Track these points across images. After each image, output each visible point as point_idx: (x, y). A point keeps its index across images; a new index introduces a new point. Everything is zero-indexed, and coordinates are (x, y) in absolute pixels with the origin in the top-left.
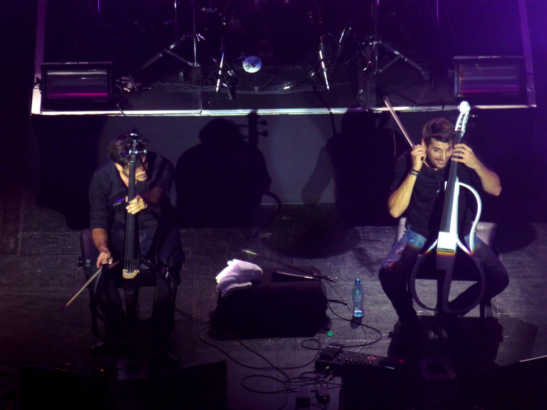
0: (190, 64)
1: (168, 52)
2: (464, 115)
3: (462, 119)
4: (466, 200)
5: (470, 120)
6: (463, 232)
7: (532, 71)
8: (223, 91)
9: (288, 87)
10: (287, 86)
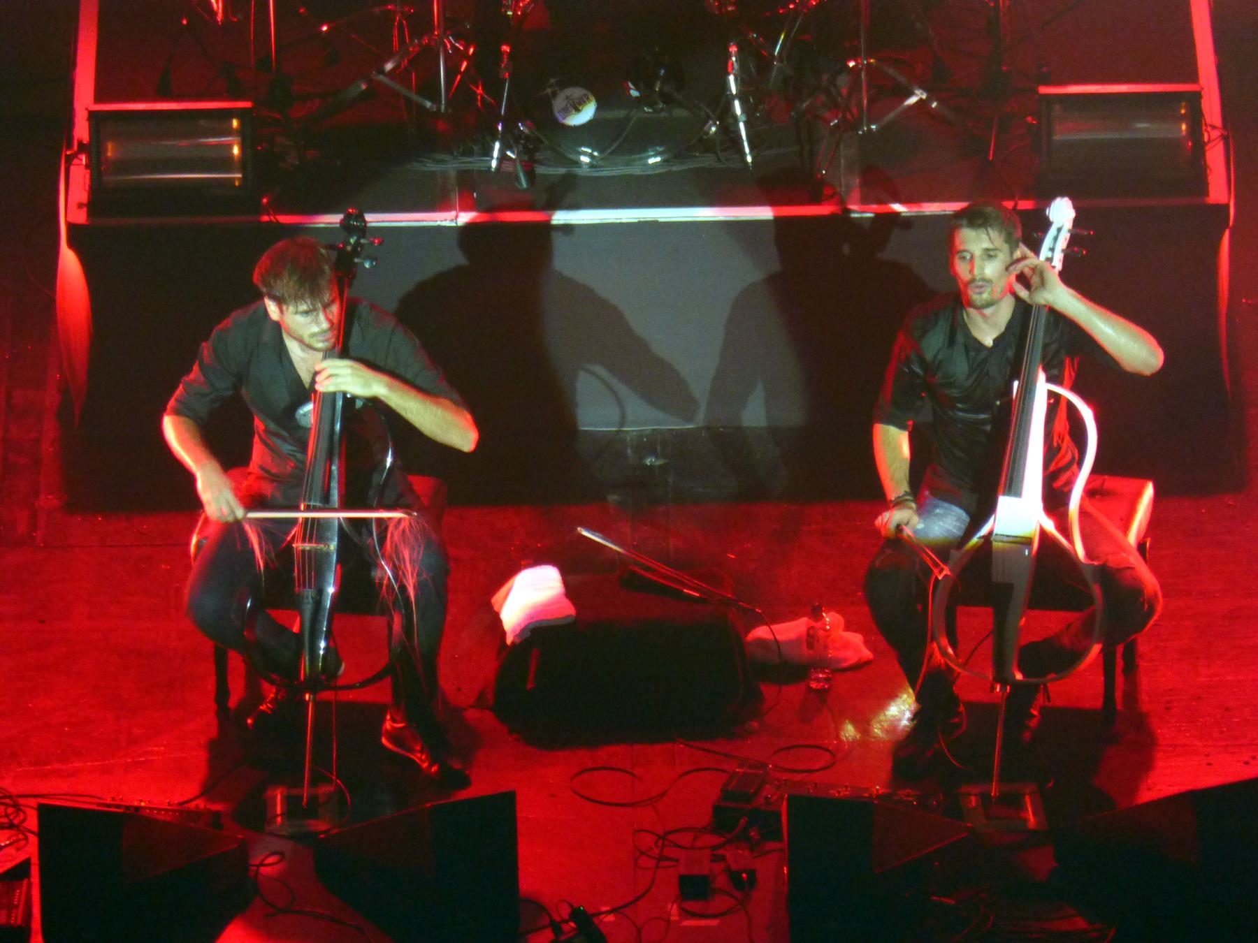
0: (428, 104)
1: (381, 77)
2: (1059, 230)
3: (1056, 239)
5: (1074, 241)
6: (1054, 500)
7: (1217, 121)
8: (508, 167)
9: (658, 159)
10: (655, 156)
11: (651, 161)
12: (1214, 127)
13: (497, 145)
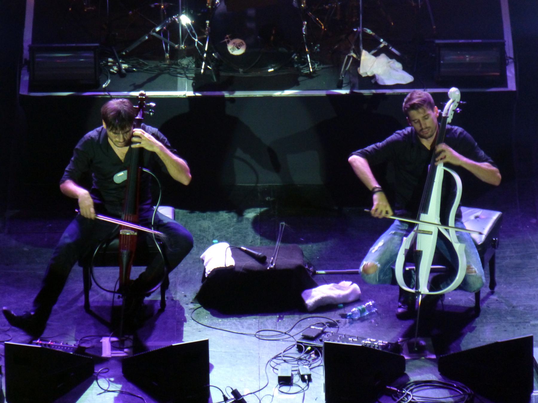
2: (453, 102)
4: (448, 182)
7: (512, 55)
8: (208, 73)
9: (272, 70)
10: (271, 68)
11: (270, 70)
12: (510, 58)
13: (204, 63)
